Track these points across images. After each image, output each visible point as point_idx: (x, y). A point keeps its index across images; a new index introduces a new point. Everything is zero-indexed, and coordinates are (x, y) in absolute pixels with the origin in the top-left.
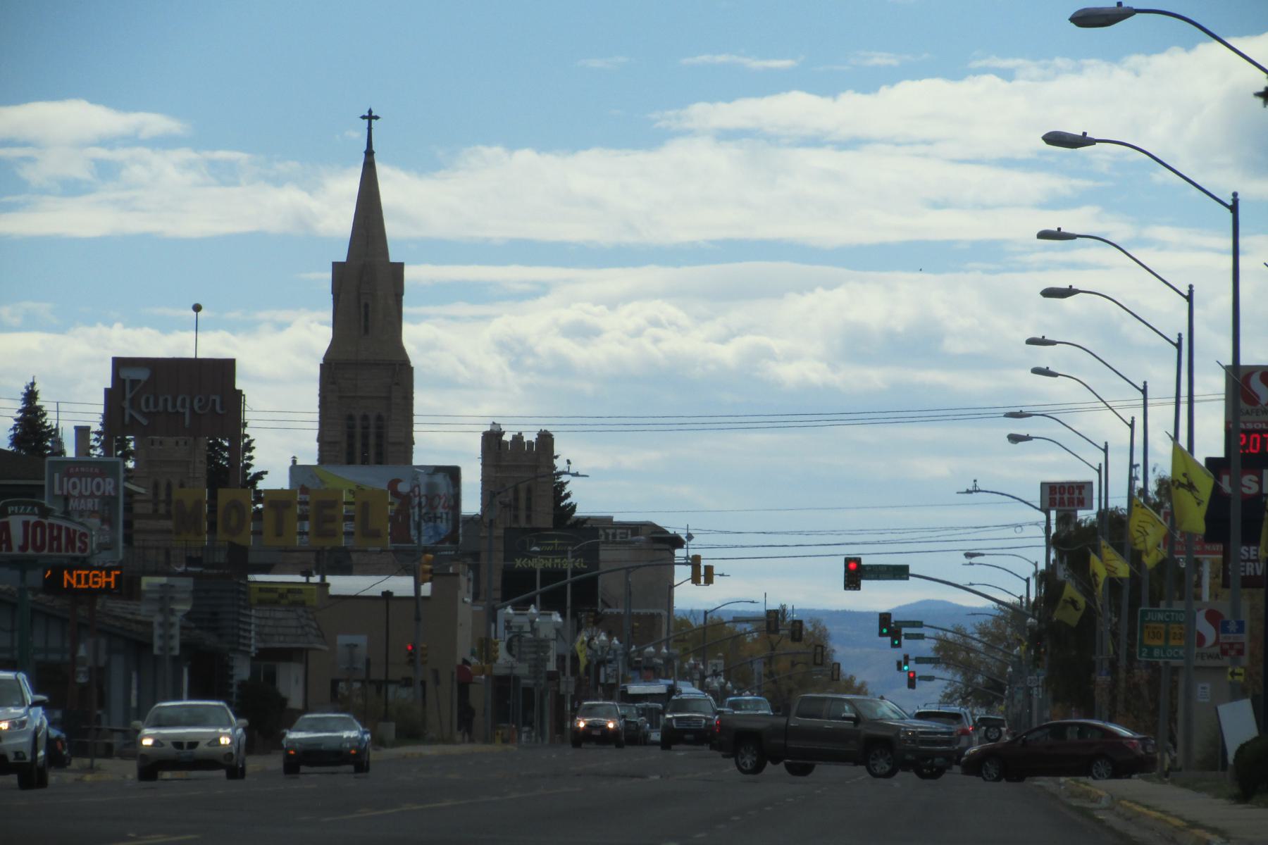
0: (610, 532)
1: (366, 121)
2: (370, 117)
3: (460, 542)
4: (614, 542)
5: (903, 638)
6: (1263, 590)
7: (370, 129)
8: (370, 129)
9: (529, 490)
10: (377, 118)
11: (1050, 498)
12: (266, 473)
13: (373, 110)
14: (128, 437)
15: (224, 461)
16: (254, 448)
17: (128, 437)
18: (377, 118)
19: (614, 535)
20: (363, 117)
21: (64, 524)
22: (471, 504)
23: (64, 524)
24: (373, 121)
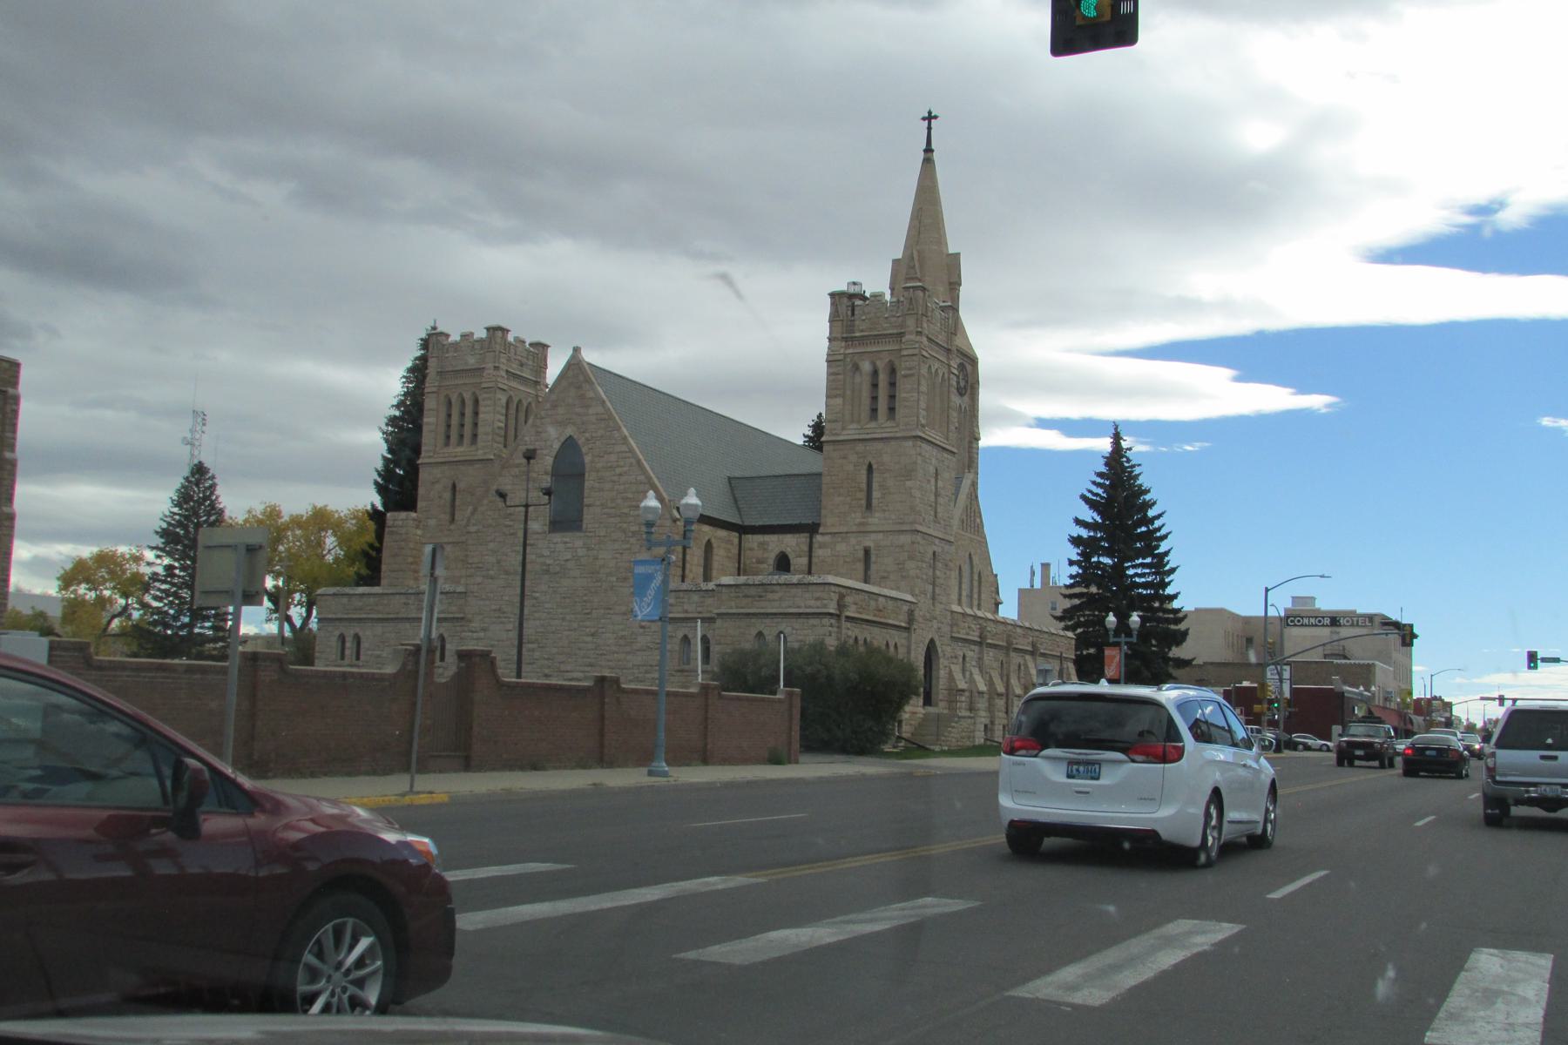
0: (1355, 619)
1: (927, 122)
2: (930, 118)
3: (433, 849)
4: (1358, 625)
5: (1539, 661)
6: (1545, 962)
7: (929, 128)
8: (929, 128)
9: (893, 371)
10: (936, 117)
11: (1126, 683)
12: (1179, 593)
13: (921, 116)
14: (1126, 565)
15: (1102, 537)
16: (1173, 570)
17: (1126, 565)
18: (936, 117)
19: (1358, 621)
20: (924, 119)
21: (973, 536)
22: (449, 906)
23: (973, 536)
24: (933, 121)
